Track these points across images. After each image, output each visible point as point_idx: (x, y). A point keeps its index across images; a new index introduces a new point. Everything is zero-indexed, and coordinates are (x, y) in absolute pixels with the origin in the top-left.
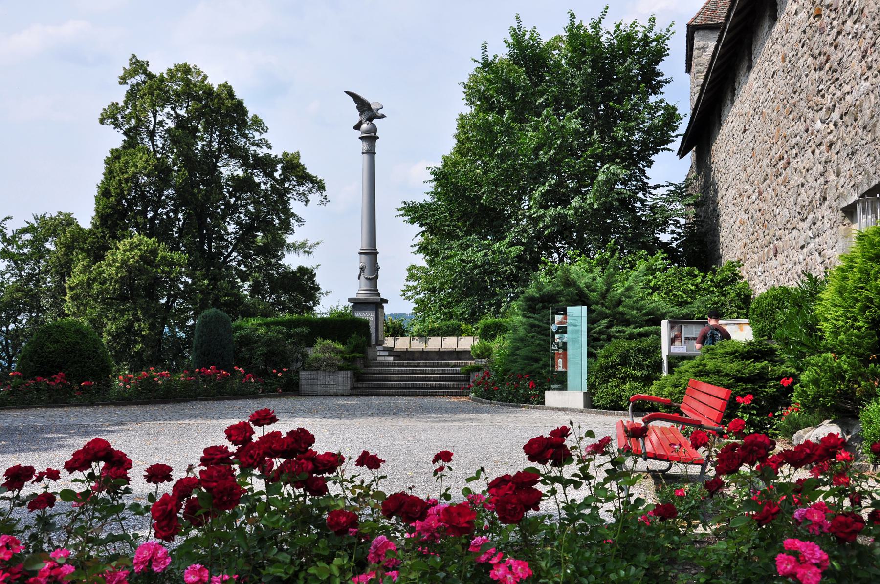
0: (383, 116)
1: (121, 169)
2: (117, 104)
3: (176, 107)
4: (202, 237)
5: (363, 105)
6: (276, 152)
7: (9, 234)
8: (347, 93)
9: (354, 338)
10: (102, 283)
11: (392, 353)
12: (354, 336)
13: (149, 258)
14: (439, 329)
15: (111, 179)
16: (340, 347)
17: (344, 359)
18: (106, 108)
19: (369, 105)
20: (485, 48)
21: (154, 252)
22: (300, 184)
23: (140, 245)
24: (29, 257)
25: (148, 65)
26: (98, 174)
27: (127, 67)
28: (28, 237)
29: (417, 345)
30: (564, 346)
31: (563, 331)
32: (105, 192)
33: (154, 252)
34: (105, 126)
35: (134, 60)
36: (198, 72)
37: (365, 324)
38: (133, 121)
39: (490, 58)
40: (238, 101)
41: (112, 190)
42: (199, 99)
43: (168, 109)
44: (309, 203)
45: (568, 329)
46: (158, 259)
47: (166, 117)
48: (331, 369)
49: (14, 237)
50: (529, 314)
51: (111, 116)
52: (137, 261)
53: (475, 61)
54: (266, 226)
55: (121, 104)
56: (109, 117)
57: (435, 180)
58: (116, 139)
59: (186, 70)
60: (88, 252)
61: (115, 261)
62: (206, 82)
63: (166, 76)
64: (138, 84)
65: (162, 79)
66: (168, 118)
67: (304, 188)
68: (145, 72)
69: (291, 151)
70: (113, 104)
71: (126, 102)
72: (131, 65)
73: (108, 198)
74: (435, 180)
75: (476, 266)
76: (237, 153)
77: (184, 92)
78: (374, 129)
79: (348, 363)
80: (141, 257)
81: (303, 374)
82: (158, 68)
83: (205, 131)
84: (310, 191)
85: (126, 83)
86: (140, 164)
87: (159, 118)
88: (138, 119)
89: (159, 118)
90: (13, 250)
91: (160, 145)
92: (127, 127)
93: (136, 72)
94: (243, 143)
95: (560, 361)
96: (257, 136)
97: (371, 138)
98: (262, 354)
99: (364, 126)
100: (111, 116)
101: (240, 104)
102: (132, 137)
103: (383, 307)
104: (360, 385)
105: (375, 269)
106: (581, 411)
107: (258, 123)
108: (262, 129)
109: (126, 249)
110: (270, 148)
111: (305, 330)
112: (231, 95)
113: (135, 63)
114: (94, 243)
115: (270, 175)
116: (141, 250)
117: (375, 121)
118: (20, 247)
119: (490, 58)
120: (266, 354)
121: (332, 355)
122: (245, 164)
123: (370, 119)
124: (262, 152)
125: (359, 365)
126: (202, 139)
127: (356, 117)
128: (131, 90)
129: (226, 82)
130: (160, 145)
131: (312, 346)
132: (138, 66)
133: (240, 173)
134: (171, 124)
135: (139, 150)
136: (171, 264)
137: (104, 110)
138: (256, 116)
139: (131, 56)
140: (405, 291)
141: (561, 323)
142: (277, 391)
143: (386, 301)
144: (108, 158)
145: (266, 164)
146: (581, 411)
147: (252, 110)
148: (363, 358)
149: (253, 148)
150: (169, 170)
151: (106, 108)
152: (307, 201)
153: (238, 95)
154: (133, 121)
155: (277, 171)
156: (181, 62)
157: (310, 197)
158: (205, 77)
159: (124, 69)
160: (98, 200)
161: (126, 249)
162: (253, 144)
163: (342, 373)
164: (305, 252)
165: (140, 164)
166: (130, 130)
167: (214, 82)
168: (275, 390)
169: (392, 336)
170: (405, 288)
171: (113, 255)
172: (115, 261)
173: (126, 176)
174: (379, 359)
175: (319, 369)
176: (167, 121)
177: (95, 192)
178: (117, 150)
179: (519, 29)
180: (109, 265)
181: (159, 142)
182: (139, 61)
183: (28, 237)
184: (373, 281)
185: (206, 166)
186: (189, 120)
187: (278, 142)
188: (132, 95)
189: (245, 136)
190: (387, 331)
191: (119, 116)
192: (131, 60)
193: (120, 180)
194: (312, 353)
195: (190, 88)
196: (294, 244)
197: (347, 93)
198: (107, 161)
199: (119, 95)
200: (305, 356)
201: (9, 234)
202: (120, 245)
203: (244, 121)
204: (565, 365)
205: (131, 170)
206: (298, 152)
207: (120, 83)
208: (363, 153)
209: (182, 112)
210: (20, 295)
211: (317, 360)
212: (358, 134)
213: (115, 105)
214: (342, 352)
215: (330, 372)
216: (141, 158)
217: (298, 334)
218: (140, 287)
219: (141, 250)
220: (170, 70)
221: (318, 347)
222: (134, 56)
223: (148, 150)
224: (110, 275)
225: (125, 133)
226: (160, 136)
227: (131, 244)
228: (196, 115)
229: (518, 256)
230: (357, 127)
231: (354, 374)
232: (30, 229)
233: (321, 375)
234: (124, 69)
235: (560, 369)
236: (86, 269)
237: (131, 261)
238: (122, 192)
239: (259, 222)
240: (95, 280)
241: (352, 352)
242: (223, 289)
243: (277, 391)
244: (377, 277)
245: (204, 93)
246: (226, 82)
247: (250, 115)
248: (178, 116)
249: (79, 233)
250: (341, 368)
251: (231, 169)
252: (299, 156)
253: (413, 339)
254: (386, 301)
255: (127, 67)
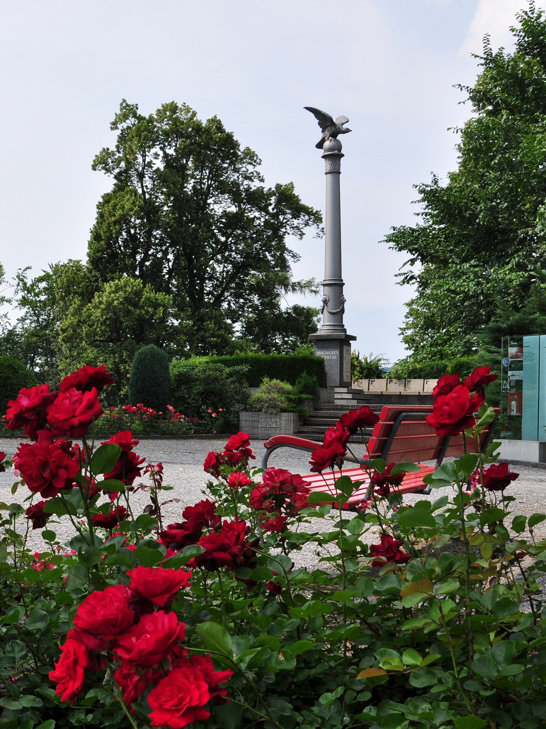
0: (348, 131)
1: (110, 212)
2: (108, 149)
3: (165, 146)
4: (192, 276)
5: (325, 121)
6: (269, 185)
7: (29, 283)
8: (307, 108)
9: (304, 378)
10: (90, 326)
11: (358, 396)
12: (304, 375)
13: (132, 301)
14: (421, 370)
15: (102, 223)
16: (288, 387)
17: (290, 400)
18: (98, 154)
19: (331, 119)
20: (487, 41)
21: (138, 293)
22: (296, 216)
23: (125, 286)
24: (44, 304)
25: (137, 108)
26: (90, 219)
27: (119, 112)
28: (43, 285)
29: (395, 388)
30: (519, 384)
31: (518, 366)
32: (96, 236)
33: (138, 293)
34: (97, 171)
35: (124, 105)
36: (188, 110)
37: (320, 363)
38: (123, 164)
39: (494, 52)
40: (228, 134)
41: (102, 234)
42: (188, 136)
43: (156, 149)
44: (304, 236)
45: (524, 363)
46: (143, 300)
47: (156, 158)
48: (274, 411)
49: (32, 286)
50: (493, 348)
51: (102, 162)
52: (121, 303)
53: (476, 56)
54: (258, 262)
55: (113, 148)
56: (100, 163)
57: (423, 200)
58: (107, 183)
59: (173, 108)
60: (82, 294)
61: (100, 303)
62: (195, 119)
63: (155, 117)
64: (128, 128)
65: (151, 120)
66: (156, 158)
67: (300, 221)
68: (135, 116)
69: (284, 182)
70: (104, 149)
71: (117, 147)
72: (121, 110)
73: (99, 242)
74: (423, 200)
75: (467, 297)
76: (224, 188)
77: (172, 131)
78: (339, 147)
79: (295, 405)
80: (125, 299)
81: (244, 416)
82: (145, 112)
83: (196, 169)
84: (307, 224)
85: (117, 128)
86: (127, 206)
87: (148, 159)
88: (128, 162)
89: (148, 159)
90: (31, 297)
91: (149, 186)
92: (117, 170)
93: (125, 117)
94: (236, 177)
95: (514, 403)
96: (250, 168)
97: (334, 157)
98: (198, 393)
99: (327, 144)
100: (102, 162)
101: (229, 137)
102: (123, 181)
103: (350, 345)
104: (305, 429)
105: (340, 301)
106: (535, 466)
107: (250, 156)
108: (255, 161)
109: (109, 293)
110: (262, 180)
111: (245, 368)
112: (220, 128)
113: (125, 108)
114: (88, 286)
115: (264, 209)
116: (125, 291)
117: (340, 137)
118: (37, 295)
119: (494, 52)
120: (203, 393)
121: (276, 396)
122: (236, 198)
123: (334, 135)
124: (255, 185)
125: (307, 408)
126: (193, 177)
127: (318, 134)
128: (122, 134)
129: (215, 117)
130: (149, 186)
131: (257, 386)
132: (128, 110)
133: (233, 209)
134: (159, 164)
135: (127, 193)
136: (156, 305)
137: (96, 156)
138: (248, 149)
139: (121, 101)
140: (404, 329)
141: (516, 356)
142: (212, 433)
143: (354, 338)
144: (100, 203)
145: (257, 198)
146: (535, 466)
147: (244, 143)
148: (313, 400)
149: (246, 182)
150: (158, 209)
151: (98, 154)
152: (302, 234)
153: (228, 129)
154: (123, 164)
155: (271, 204)
156: (168, 102)
157: (306, 230)
158: (194, 114)
159: (116, 114)
160: (90, 244)
161: (109, 293)
162: (246, 178)
163: (285, 416)
164: (312, 291)
165: (127, 206)
166: (120, 174)
167: (203, 118)
168: (209, 432)
169: (366, 377)
170: (404, 326)
171: (99, 297)
172: (100, 303)
173: (113, 219)
174: (338, 402)
175: (260, 410)
176: (154, 161)
177: (88, 237)
178: (108, 194)
179: (532, 12)
180: (96, 307)
181: (148, 183)
182: (128, 105)
183: (43, 285)
184: (338, 316)
185: (195, 206)
186: (177, 159)
187: (270, 175)
188: (122, 139)
189: (236, 170)
190: (361, 373)
191: (110, 161)
192: (121, 104)
193: (109, 224)
194: (257, 393)
195: (176, 126)
196: (299, 283)
197: (307, 108)
198: (100, 206)
199: (111, 140)
200: (247, 396)
201: (29, 283)
202: (107, 286)
203: (235, 154)
204: (520, 408)
205: (119, 213)
206: (292, 183)
207: (112, 129)
208: (326, 174)
209: (171, 151)
210: (35, 339)
211: (259, 400)
212: (321, 152)
213: (106, 151)
214: (289, 393)
215: (271, 413)
216: (128, 200)
217: (238, 372)
218: (130, 327)
219: (125, 291)
220: (159, 110)
221: (263, 387)
222: (124, 101)
223: (136, 193)
224: (97, 317)
225: (116, 177)
226: (150, 178)
227: (117, 285)
228: (184, 153)
229: (521, 285)
230: (320, 145)
231: (300, 416)
232: (46, 278)
233: (262, 416)
234: (116, 114)
235: (514, 413)
236: (78, 311)
237: (116, 303)
238: (111, 235)
239: (253, 260)
240: (84, 322)
241: (301, 393)
242: (209, 330)
243: (212, 433)
244: (343, 311)
245: (193, 129)
246: (215, 117)
247: (242, 148)
248: (166, 155)
249: (74, 278)
250: (283, 410)
251: (220, 206)
252: (293, 187)
253: (391, 381)
254: (354, 338)
255: (119, 112)
